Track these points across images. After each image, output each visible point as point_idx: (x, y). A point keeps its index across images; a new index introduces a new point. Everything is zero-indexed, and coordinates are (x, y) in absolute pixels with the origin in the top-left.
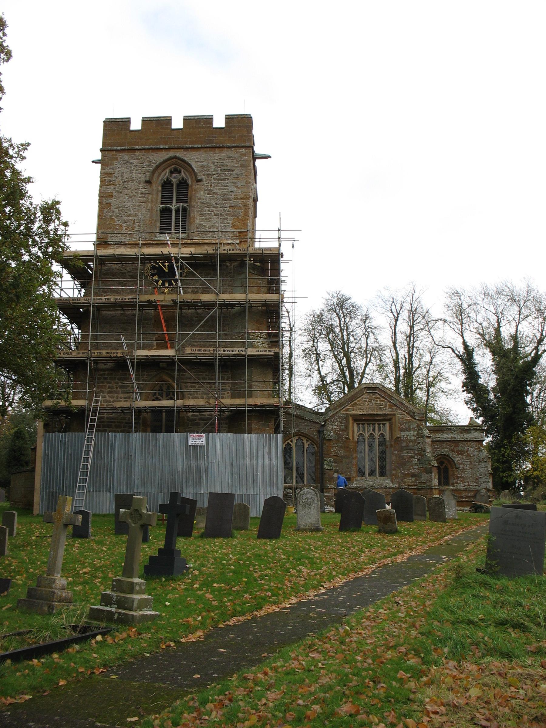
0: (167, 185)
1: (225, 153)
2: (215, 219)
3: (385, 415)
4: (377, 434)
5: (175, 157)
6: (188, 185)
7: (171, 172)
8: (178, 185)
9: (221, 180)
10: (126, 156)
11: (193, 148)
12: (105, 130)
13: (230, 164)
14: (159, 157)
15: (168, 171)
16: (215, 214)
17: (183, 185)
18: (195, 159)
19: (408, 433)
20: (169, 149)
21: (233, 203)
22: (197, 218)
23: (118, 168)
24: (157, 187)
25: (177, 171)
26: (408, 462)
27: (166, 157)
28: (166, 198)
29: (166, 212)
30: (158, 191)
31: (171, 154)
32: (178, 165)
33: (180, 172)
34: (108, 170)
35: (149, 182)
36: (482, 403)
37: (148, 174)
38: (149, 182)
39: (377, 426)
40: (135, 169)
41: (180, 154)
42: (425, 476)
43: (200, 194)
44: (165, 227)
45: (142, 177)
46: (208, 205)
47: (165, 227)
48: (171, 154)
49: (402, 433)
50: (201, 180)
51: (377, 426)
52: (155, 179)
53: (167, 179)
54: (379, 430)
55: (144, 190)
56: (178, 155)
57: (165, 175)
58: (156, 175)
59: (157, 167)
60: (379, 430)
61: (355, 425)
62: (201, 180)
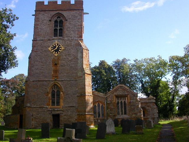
0: (56, 22)
1: (74, 12)
2: (72, 32)
3: (125, 95)
4: (123, 101)
5: (59, 13)
6: (63, 22)
7: (57, 18)
8: (60, 22)
9: (73, 20)
10: (43, 13)
11: (53, 10)
12: (83, 4)
13: (76, 15)
14: (54, 13)
15: (56, 17)
16: (72, 31)
17: (61, 22)
18: (65, 13)
19: (133, 100)
20: (57, 10)
21: (77, 27)
22: (66, 32)
23: (41, 16)
24: (53, 22)
25: (59, 17)
26: (133, 110)
27: (56, 13)
28: (56, 26)
29: (56, 30)
30: (53, 23)
31: (58, 12)
32: (59, 15)
33: (60, 18)
34: (37, 17)
35: (50, 21)
36: (153, 94)
37: (50, 18)
38: (50, 21)
39: (120, 98)
40: (45, 17)
41: (60, 12)
42: (139, 114)
43: (67, 25)
44: (55, 35)
45: (48, 19)
46: (69, 28)
47: (55, 35)
48: (58, 12)
49: (131, 100)
50: (67, 20)
51: (120, 98)
52: (52, 19)
53: (56, 20)
54: (121, 100)
55: (49, 23)
56: (60, 12)
57: (55, 18)
58: (52, 19)
59: (53, 16)
60: (121, 100)
61: (116, 98)
62: (67, 20)
